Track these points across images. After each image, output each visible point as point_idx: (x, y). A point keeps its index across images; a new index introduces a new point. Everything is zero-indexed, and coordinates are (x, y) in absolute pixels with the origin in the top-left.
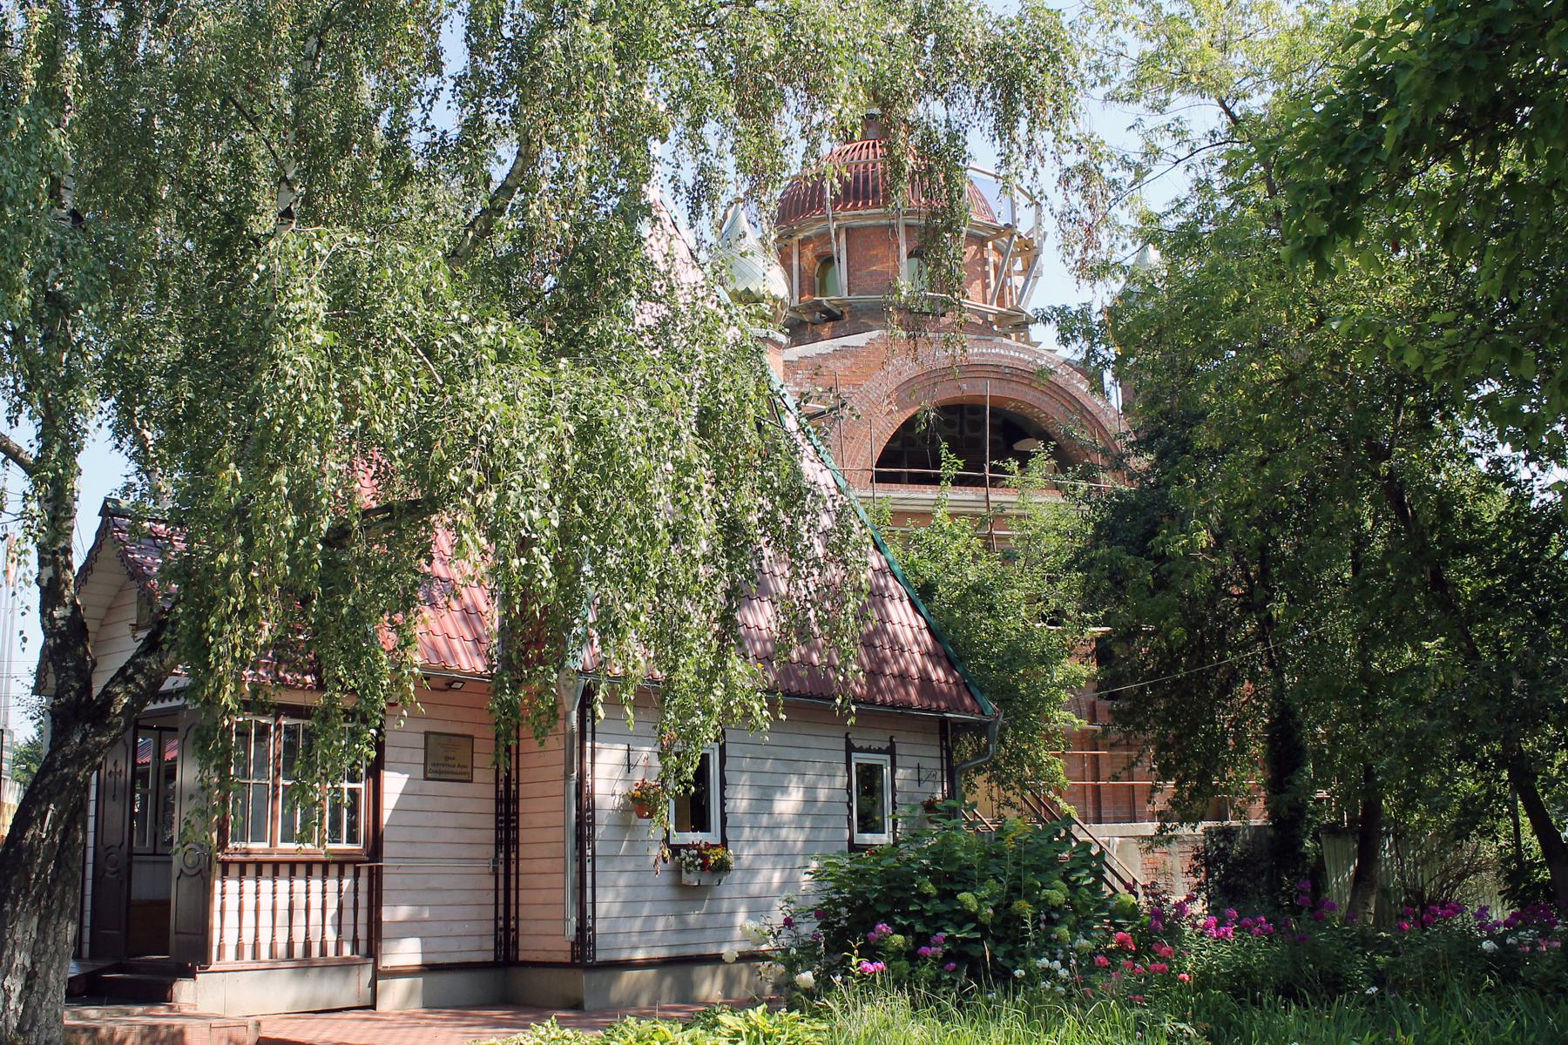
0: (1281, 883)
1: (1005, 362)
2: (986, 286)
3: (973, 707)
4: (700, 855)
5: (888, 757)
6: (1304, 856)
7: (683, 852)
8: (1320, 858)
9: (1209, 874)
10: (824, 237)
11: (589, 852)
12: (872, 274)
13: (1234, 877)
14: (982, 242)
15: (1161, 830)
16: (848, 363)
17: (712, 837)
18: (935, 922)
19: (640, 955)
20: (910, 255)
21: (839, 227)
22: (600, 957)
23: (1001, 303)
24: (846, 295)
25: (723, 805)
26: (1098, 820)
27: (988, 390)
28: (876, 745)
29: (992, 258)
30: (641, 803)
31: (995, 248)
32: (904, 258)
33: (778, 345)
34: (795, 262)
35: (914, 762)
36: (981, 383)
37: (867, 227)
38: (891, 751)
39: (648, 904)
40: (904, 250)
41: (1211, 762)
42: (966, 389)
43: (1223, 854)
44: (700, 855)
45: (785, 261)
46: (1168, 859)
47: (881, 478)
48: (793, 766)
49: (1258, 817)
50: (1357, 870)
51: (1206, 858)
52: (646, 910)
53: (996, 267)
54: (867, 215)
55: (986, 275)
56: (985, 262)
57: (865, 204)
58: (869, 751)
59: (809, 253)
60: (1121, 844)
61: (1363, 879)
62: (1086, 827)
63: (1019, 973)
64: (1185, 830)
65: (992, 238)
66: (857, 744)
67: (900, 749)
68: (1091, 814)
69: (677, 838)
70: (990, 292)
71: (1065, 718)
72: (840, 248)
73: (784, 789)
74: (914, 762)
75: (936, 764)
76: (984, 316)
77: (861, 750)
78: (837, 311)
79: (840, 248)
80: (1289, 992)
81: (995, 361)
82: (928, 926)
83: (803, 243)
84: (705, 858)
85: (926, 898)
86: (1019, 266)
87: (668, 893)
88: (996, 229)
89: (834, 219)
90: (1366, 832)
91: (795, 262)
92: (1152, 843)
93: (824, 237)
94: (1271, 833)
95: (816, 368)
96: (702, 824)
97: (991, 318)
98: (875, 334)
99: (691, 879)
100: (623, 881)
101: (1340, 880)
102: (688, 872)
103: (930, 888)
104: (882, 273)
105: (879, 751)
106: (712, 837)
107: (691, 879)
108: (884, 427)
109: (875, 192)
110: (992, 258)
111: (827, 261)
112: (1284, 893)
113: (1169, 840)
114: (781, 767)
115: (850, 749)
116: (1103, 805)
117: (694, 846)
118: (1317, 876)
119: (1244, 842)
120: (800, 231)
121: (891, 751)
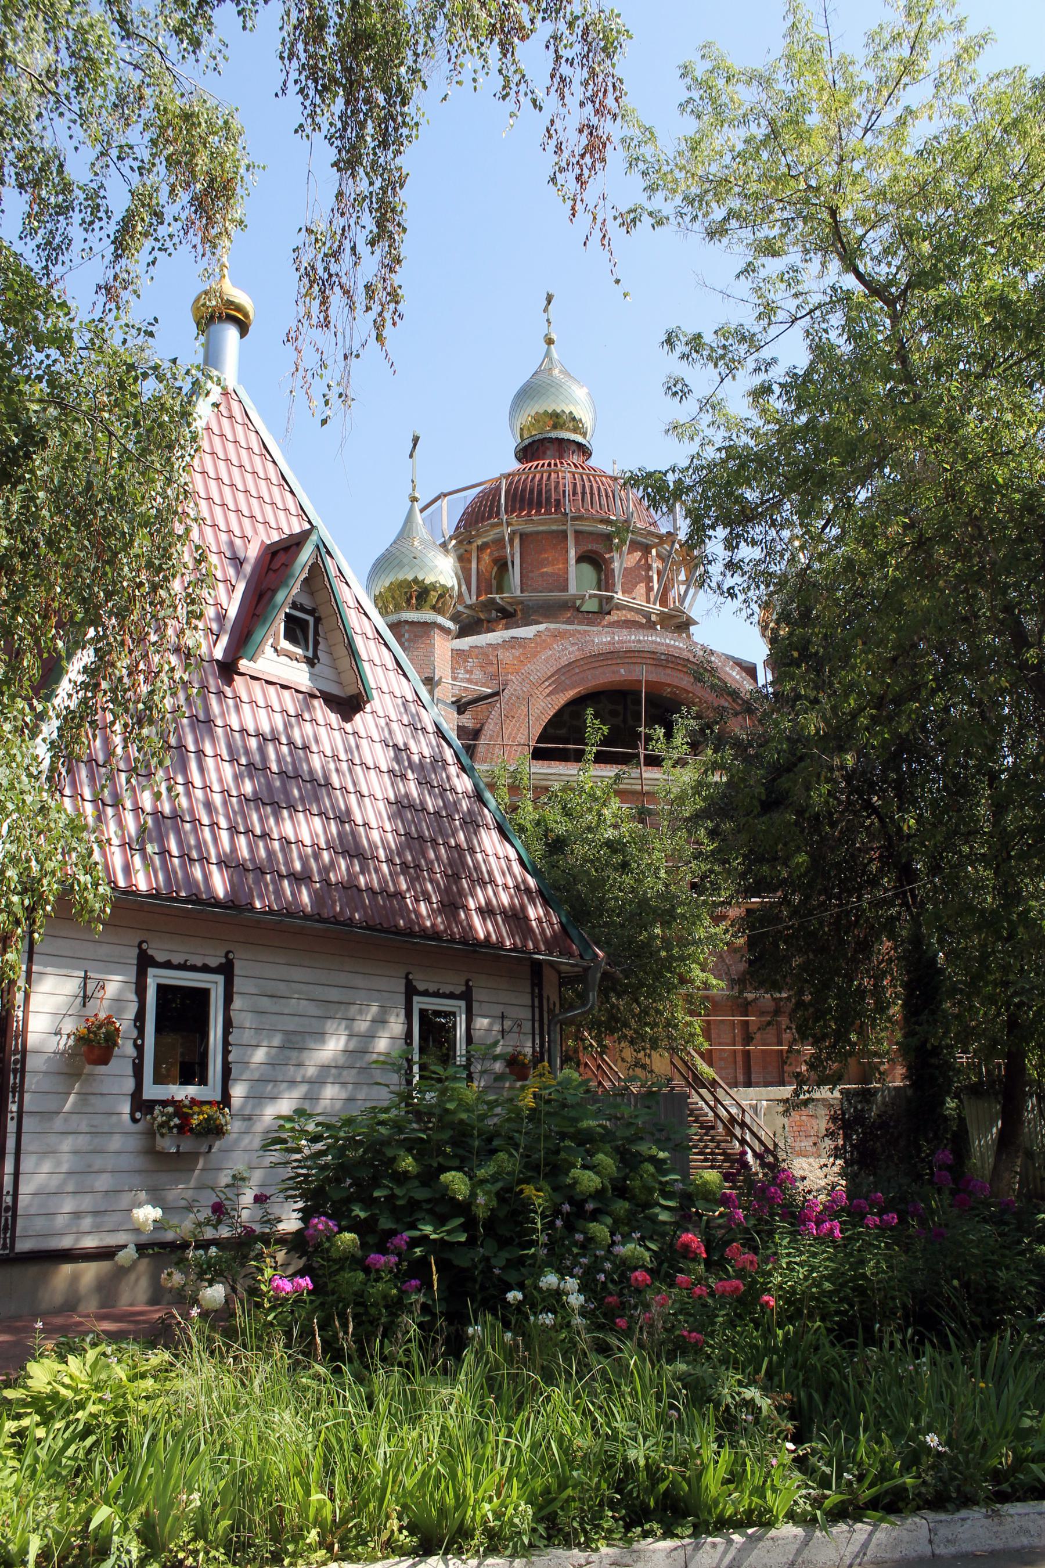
0: (919, 1149)
1: (662, 649)
2: (649, 589)
3: (591, 955)
4: (176, 1114)
5: (462, 1004)
6: (946, 1119)
7: (157, 1109)
8: (962, 1120)
9: (847, 1137)
10: (499, 542)
11: (14, 1108)
12: (542, 575)
13: (864, 1138)
14: (646, 549)
15: (796, 1093)
16: (517, 653)
17: (211, 1092)
18: (408, 1213)
19: (89, 1242)
20: (580, 560)
21: (513, 533)
22: (23, 1246)
23: (664, 602)
24: (518, 593)
25: (226, 1052)
26: (748, 1084)
27: (644, 674)
28: (446, 989)
29: (656, 565)
30: (94, 1045)
31: (658, 555)
32: (572, 561)
33: (446, 631)
34: (474, 565)
35: (498, 1010)
36: (637, 668)
37: (538, 533)
38: (467, 996)
39: (105, 1176)
40: (572, 554)
41: (850, 1016)
42: (622, 674)
43: (859, 1118)
44: (176, 1114)
45: (463, 559)
46: (814, 1122)
47: (539, 755)
48: (335, 1009)
49: (897, 1078)
50: (1001, 1132)
51: (843, 1119)
52: (103, 1182)
53: (659, 573)
54: (539, 523)
55: (650, 579)
56: (649, 567)
57: (538, 513)
58: (436, 994)
59: (486, 557)
60: (768, 1107)
61: (1006, 1141)
62: (733, 1092)
63: (514, 1296)
64: (824, 1092)
65: (656, 546)
66: (421, 986)
67: (477, 994)
68: (741, 1078)
69: (152, 1091)
70: (652, 595)
71: (705, 976)
72: (514, 553)
73: (321, 1036)
74: (498, 1010)
75: (525, 1014)
76: (647, 615)
77: (426, 993)
78: (510, 609)
79: (514, 553)
80: (925, 1321)
81: (652, 648)
82: (398, 1221)
83: (481, 549)
84: (186, 1118)
85: (402, 1178)
86: (682, 577)
87: (139, 1162)
88: (660, 537)
89: (509, 524)
90: (1009, 1092)
91: (474, 565)
92: (790, 1106)
93: (499, 542)
94: (910, 1092)
95: (482, 654)
96: (193, 1072)
97: (654, 618)
98: (542, 627)
99: (168, 1144)
100: (67, 1144)
101: (984, 1140)
102: (162, 1135)
103: (408, 1163)
104: (552, 574)
105: (451, 996)
106: (211, 1092)
107: (168, 1144)
108: (545, 707)
109: (548, 499)
110: (656, 565)
111: (502, 565)
112: (923, 1160)
113: (806, 1103)
114: (312, 1009)
115: (411, 991)
116: (754, 1069)
117: (172, 1102)
118: (960, 1143)
119: (884, 1103)
120: (478, 536)
121: (467, 996)
